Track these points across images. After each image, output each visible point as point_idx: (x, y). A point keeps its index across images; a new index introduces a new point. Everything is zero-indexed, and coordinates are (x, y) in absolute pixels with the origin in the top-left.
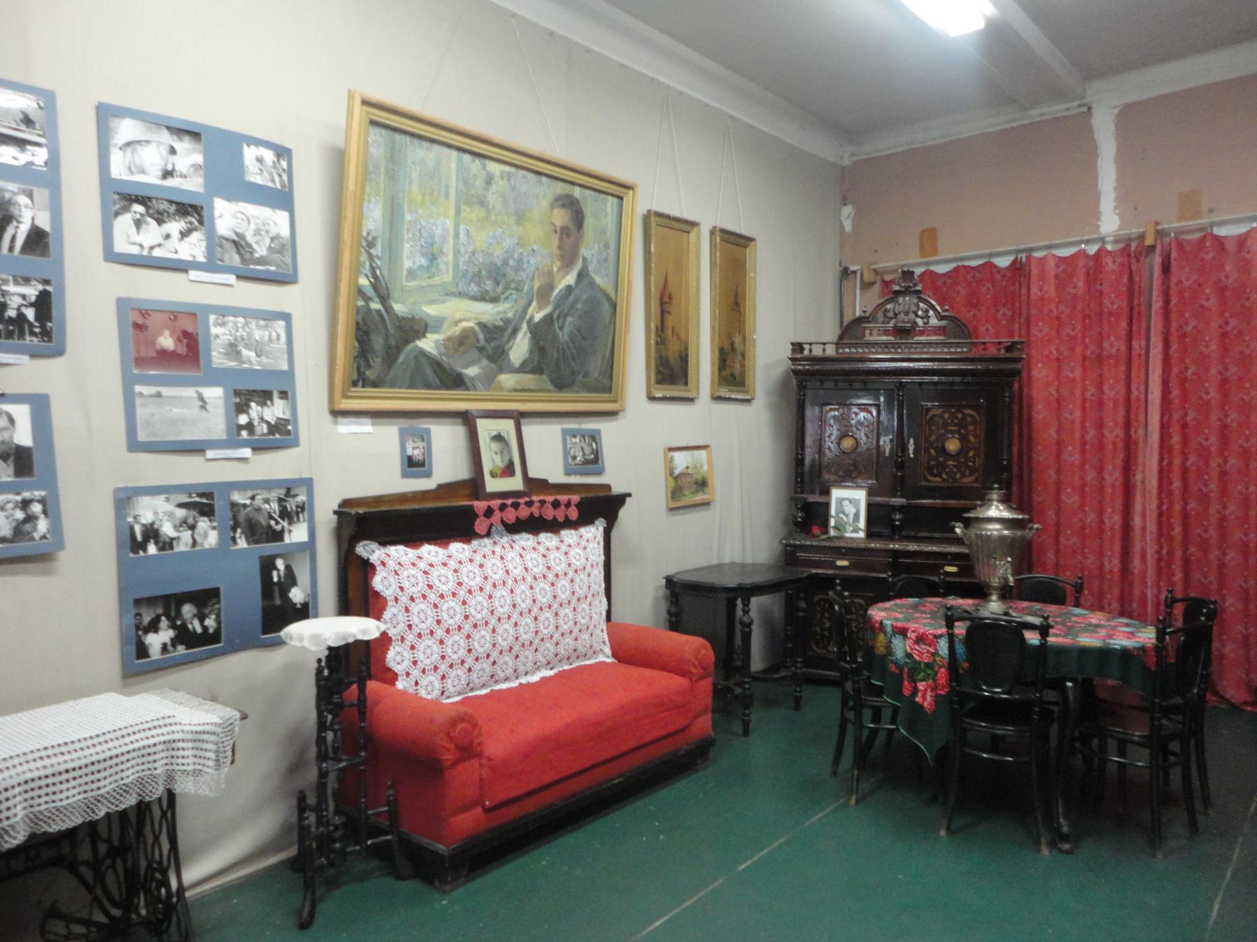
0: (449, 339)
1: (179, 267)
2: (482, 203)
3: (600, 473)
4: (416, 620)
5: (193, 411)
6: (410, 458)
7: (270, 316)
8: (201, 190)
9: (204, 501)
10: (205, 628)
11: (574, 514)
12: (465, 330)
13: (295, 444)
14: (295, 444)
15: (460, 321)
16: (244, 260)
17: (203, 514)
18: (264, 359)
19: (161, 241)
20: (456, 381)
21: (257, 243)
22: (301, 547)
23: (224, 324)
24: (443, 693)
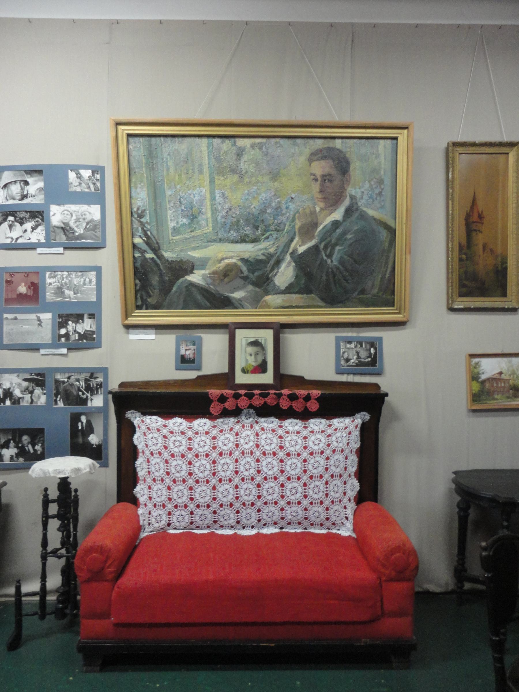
0: (214, 273)
1: (32, 247)
2: (233, 171)
3: (379, 374)
4: (153, 469)
5: (34, 327)
6: (183, 357)
7: (84, 270)
8: (43, 202)
9: (39, 378)
10: (35, 451)
11: (313, 406)
12: (228, 265)
13: (99, 346)
14: (99, 346)
15: (223, 259)
16: (68, 238)
17: (38, 385)
18: (79, 295)
19: (22, 234)
20: (224, 303)
21: (77, 227)
22: (98, 410)
23: (55, 277)
24: (169, 525)
